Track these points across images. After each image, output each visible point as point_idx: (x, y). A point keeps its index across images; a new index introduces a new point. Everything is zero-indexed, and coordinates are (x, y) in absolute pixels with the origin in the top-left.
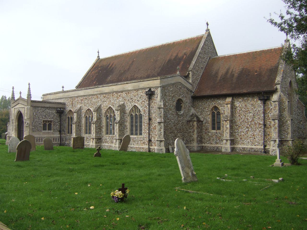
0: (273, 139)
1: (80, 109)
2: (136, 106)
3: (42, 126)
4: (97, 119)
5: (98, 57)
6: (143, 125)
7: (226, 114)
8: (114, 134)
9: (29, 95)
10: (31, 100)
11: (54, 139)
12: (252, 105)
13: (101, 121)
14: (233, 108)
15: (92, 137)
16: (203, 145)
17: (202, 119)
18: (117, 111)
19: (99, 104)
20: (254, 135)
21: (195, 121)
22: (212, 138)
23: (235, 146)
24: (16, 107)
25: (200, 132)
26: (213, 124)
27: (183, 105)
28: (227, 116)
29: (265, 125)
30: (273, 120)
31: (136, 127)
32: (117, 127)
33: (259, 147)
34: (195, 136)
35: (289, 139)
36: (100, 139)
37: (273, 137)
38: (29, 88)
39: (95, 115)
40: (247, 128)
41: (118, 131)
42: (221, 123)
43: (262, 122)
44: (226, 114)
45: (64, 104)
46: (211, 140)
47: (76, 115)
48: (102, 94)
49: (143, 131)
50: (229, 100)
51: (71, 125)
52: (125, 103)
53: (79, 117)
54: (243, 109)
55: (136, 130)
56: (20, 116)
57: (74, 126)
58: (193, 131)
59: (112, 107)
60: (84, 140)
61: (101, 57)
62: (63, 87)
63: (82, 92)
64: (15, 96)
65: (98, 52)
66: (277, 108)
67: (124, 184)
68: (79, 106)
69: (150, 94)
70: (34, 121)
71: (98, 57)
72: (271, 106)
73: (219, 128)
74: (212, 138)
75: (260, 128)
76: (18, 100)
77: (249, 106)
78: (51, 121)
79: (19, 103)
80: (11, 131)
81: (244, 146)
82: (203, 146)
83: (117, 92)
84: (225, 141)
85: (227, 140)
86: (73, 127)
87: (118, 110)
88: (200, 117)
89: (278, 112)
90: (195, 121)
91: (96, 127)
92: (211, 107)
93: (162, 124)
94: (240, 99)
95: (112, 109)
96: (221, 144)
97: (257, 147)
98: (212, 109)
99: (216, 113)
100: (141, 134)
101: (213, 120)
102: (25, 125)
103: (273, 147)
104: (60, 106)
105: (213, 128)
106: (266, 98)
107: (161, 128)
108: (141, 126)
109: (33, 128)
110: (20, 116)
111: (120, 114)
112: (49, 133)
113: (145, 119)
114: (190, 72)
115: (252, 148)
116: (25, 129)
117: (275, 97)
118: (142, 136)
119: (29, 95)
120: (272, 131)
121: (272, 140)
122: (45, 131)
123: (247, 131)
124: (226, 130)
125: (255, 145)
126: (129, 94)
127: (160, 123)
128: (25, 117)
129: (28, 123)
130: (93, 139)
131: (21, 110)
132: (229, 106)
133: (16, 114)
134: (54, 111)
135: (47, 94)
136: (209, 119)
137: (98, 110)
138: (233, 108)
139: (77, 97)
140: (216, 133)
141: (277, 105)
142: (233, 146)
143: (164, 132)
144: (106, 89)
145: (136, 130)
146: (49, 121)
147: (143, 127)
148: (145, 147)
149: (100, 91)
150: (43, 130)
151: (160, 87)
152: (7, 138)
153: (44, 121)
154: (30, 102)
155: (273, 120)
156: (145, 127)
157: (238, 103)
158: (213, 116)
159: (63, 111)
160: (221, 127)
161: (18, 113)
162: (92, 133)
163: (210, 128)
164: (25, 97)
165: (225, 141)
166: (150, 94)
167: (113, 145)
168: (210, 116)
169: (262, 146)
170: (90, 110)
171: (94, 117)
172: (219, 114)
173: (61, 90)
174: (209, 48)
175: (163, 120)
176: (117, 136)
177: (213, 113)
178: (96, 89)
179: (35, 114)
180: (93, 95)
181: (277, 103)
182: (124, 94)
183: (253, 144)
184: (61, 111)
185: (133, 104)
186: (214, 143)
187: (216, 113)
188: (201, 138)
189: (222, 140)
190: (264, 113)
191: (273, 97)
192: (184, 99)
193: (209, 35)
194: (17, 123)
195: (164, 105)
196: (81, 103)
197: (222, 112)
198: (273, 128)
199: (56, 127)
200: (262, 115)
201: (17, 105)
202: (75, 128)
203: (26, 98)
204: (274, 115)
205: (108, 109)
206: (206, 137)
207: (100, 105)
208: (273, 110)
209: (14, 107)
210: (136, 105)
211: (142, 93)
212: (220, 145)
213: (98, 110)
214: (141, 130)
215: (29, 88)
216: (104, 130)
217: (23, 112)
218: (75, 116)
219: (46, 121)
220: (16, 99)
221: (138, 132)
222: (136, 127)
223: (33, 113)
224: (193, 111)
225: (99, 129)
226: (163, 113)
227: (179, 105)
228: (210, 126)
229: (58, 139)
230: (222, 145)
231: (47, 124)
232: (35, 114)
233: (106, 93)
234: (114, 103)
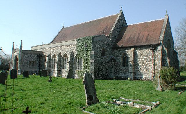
1: (50, 55)
3: (29, 64)
5: (63, 27)
9: (21, 47)
10: (23, 49)
11: (35, 71)
12: (146, 52)
13: (61, 61)
14: (135, 55)
17: (117, 61)
19: (59, 52)
22: (123, 72)
23: (136, 76)
24: (14, 54)
26: (124, 63)
27: (106, 52)
29: (154, 64)
30: (158, 61)
33: (150, 77)
34: (113, 70)
38: (21, 43)
43: (151, 63)
45: (42, 52)
48: (61, 46)
50: (132, 49)
52: (74, 52)
58: (112, 68)
59: (66, 53)
62: (43, 43)
63: (51, 46)
64: (14, 48)
65: (63, 24)
66: (161, 54)
67: (28, 107)
68: (49, 53)
71: (63, 27)
72: (157, 53)
73: (127, 66)
74: (123, 72)
76: (16, 49)
77: (144, 53)
78: (34, 61)
83: (69, 45)
84: (130, 73)
85: (131, 73)
88: (116, 59)
89: (161, 57)
91: (57, 64)
92: (122, 54)
98: (123, 55)
101: (124, 61)
104: (40, 53)
105: (124, 66)
106: (154, 48)
111: (70, 57)
114: (111, 34)
117: (160, 48)
119: (21, 47)
124: (131, 67)
127: (91, 63)
128: (19, 60)
131: (17, 55)
132: (132, 53)
133: (14, 57)
134: (36, 56)
135: (33, 47)
136: (121, 60)
137: (60, 55)
138: (135, 55)
141: (161, 53)
144: (64, 43)
146: (33, 61)
155: (158, 61)
157: (138, 51)
159: (41, 56)
160: (128, 65)
164: (19, 47)
165: (130, 73)
173: (42, 44)
174: (122, 21)
178: (58, 44)
181: (161, 51)
184: (40, 56)
189: (128, 73)
191: (158, 48)
193: (122, 13)
199: (37, 64)
200: (152, 58)
203: (20, 49)
206: (119, 71)
207: (60, 53)
214: (81, 67)
215: (21, 43)
218: (47, 58)
220: (15, 49)
221: (80, 67)
224: (112, 56)
226: (93, 57)
227: (103, 53)
228: (121, 64)
229: (38, 72)
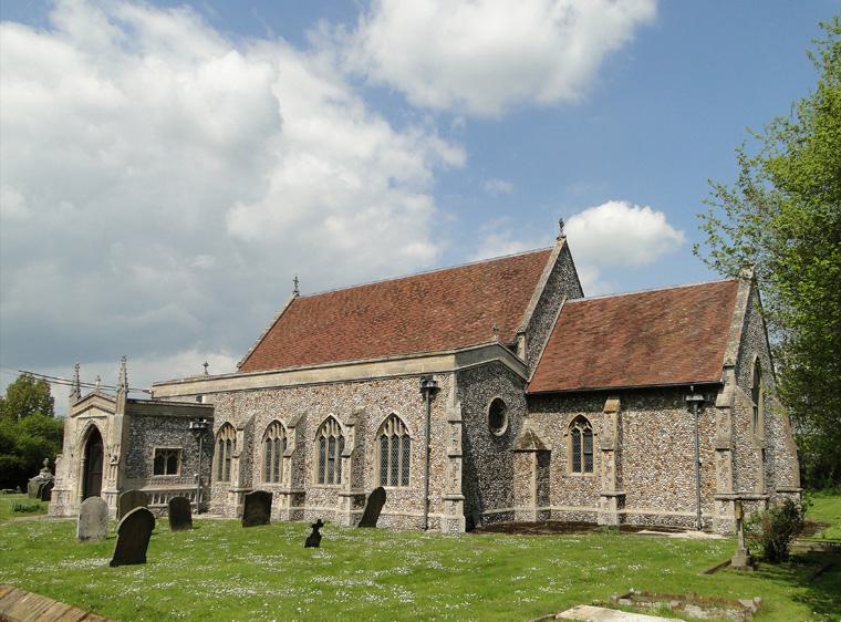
0: (718, 496)
1: (252, 422)
2: (396, 416)
4: (298, 448)
6: (411, 461)
7: (607, 434)
8: (339, 482)
15: (283, 490)
16: (552, 507)
17: (549, 447)
18: (348, 428)
19: (303, 411)
20: (672, 486)
21: (532, 451)
25: (543, 479)
26: (576, 459)
28: (608, 440)
31: (395, 465)
32: (349, 467)
34: (533, 488)
35: (758, 496)
36: (303, 494)
37: (719, 490)
39: (291, 435)
40: (657, 468)
41: (348, 476)
42: (594, 456)
44: (607, 434)
46: (570, 497)
47: (242, 436)
49: (411, 476)
51: (228, 460)
53: (249, 443)
54: (646, 424)
55: (395, 473)
56: (93, 438)
57: (235, 463)
58: (528, 477)
59: (335, 417)
60: (116, 553)
61: (305, 292)
68: (250, 413)
69: (430, 392)
70: (130, 452)
72: (714, 416)
73: (589, 468)
75: (687, 468)
78: (176, 451)
79: (92, 406)
80: (65, 477)
81: (650, 513)
82: (549, 511)
86: (233, 466)
87: (351, 426)
88: (544, 441)
90: (532, 451)
93: (459, 461)
94: (640, 399)
95: (335, 421)
96: (595, 507)
97: (680, 513)
98: (572, 424)
99: (582, 432)
100: (405, 483)
101: (576, 448)
102: (107, 461)
103: (721, 513)
105: (577, 468)
107: (455, 469)
108: (406, 463)
109: (129, 467)
110: (93, 438)
112: (168, 479)
113: (417, 448)
115: (670, 517)
116: (106, 470)
118: (409, 488)
120: (718, 476)
121: (718, 499)
122: (160, 476)
123: (656, 475)
125: (677, 510)
126: (378, 389)
129: (116, 458)
130: (286, 494)
137: (299, 424)
139: (247, 391)
140: (583, 479)
142: (622, 511)
143: (463, 477)
145: (395, 473)
146: (170, 451)
147: (411, 465)
148: (414, 514)
149: (306, 379)
150: (155, 474)
151: (455, 372)
152: (54, 495)
153: (157, 451)
154: (123, 403)
156: (416, 464)
158: (576, 440)
161: (88, 430)
162: (284, 480)
163: (568, 466)
166: (430, 392)
167: (337, 509)
168: (569, 439)
169: (692, 511)
170: (280, 424)
171: (288, 441)
172: (588, 433)
175: (460, 449)
176: (348, 487)
177: (576, 431)
179: (134, 433)
180: (287, 387)
182: (365, 387)
183: (670, 505)
185: (388, 411)
186: (577, 502)
187: (582, 432)
188: (547, 490)
190: (429, 426)
192: (507, 400)
193: (565, 249)
194: (83, 457)
195: (464, 414)
196: (256, 406)
197: (595, 430)
198: (719, 470)
201: (86, 410)
202: (238, 467)
204: (720, 440)
205: (325, 422)
207: (305, 415)
208: (718, 426)
209: (77, 414)
210: (396, 413)
211: (414, 386)
212: (591, 509)
213: (299, 424)
214: (406, 473)
216: (313, 472)
217: (101, 428)
219: (163, 451)
222: (395, 465)
223: (132, 431)
225: (299, 470)
230: (596, 510)
231: (166, 458)
232: (134, 433)
233: (320, 384)
234: (342, 405)
